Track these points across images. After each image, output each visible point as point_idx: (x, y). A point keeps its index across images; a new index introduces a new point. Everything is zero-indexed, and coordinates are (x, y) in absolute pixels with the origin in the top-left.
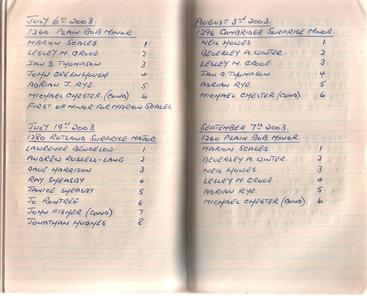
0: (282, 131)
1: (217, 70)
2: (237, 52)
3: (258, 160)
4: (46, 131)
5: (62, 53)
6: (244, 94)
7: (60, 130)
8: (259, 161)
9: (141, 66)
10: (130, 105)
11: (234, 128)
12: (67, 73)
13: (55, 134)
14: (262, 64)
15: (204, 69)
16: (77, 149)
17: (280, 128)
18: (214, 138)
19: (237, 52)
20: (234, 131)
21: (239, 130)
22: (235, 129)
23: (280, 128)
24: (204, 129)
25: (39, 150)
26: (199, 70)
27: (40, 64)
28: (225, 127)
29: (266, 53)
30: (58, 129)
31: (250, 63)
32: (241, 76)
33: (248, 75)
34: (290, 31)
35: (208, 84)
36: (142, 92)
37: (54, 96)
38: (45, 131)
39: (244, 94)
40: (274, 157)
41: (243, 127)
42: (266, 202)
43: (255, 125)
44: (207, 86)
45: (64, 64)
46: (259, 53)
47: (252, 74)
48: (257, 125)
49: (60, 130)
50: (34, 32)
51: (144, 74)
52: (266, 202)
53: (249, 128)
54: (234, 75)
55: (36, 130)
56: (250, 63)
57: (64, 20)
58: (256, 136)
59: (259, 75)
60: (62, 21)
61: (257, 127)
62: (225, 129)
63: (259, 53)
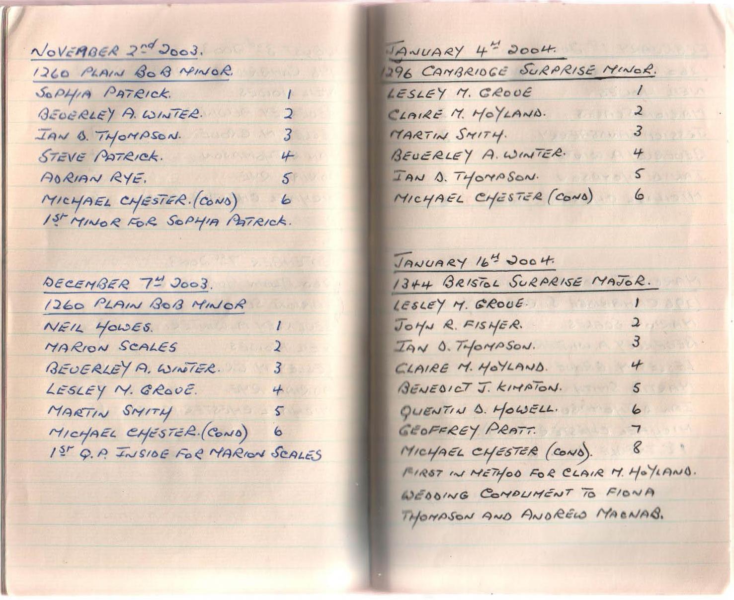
0: (202, 290)
1: (431, 168)
2: (128, 177)
3: (507, 155)
4: (462, 270)
5: (53, 408)
6: (479, 449)
7: (91, 289)
8: (508, 158)
9: (455, 137)
10: (496, 424)
11: (107, 285)
12: (488, 471)
13: (636, 74)
14: (517, 94)
15: (402, 165)
16: (407, 388)
17: (197, 285)
18: (73, 303)
19: (128, 177)
20: (107, 290)
21: (116, 288)
22: (109, 287)
23: (197, 285)
24: (516, 283)
25: (121, 330)
26: (391, 167)
27: (60, 136)
28: (89, 283)
29: (530, 154)
30: (479, 267)
31: (491, 93)
32: (546, 389)
33: (494, 179)
34: (69, 177)
35: (58, 176)
36: (283, 190)
37: (100, 433)
38: (460, 269)
39: (127, 198)
40: (194, 363)
41: (554, 281)
42: (446, 411)
43: (151, 279)
44: (225, 203)
45: (108, 137)
46: (153, 116)
47: (502, 176)
48: (154, 279)
49: (91, 289)
50: (57, 304)
51: (484, 53)
52: (446, 411)
53: (137, 284)
54: (465, 178)
55: (430, 269)
56: (491, 93)
57: (497, 45)
58: (158, 301)
59: (516, 179)
60: (493, 46)
61: (154, 282)
62: (89, 286)
63: (153, 116)
